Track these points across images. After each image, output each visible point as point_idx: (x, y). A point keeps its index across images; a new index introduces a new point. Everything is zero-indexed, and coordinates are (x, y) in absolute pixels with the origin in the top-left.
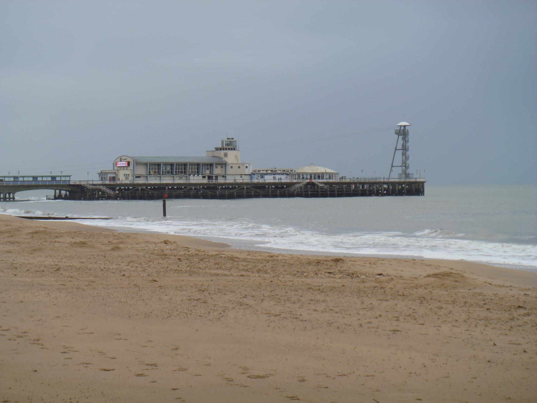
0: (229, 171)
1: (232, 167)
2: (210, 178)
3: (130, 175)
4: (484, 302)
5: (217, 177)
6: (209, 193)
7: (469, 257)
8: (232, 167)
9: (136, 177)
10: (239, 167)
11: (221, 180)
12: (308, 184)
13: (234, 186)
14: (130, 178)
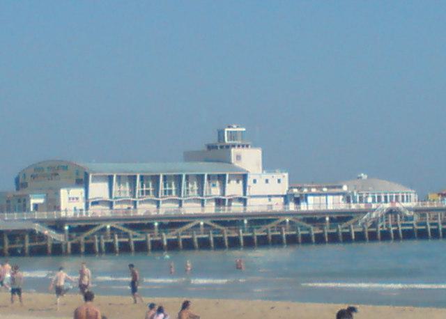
0: (253, 189)
1: (255, 181)
2: (219, 202)
8: (255, 181)
10: (267, 181)
11: (237, 208)
12: (390, 211)
13: (259, 220)
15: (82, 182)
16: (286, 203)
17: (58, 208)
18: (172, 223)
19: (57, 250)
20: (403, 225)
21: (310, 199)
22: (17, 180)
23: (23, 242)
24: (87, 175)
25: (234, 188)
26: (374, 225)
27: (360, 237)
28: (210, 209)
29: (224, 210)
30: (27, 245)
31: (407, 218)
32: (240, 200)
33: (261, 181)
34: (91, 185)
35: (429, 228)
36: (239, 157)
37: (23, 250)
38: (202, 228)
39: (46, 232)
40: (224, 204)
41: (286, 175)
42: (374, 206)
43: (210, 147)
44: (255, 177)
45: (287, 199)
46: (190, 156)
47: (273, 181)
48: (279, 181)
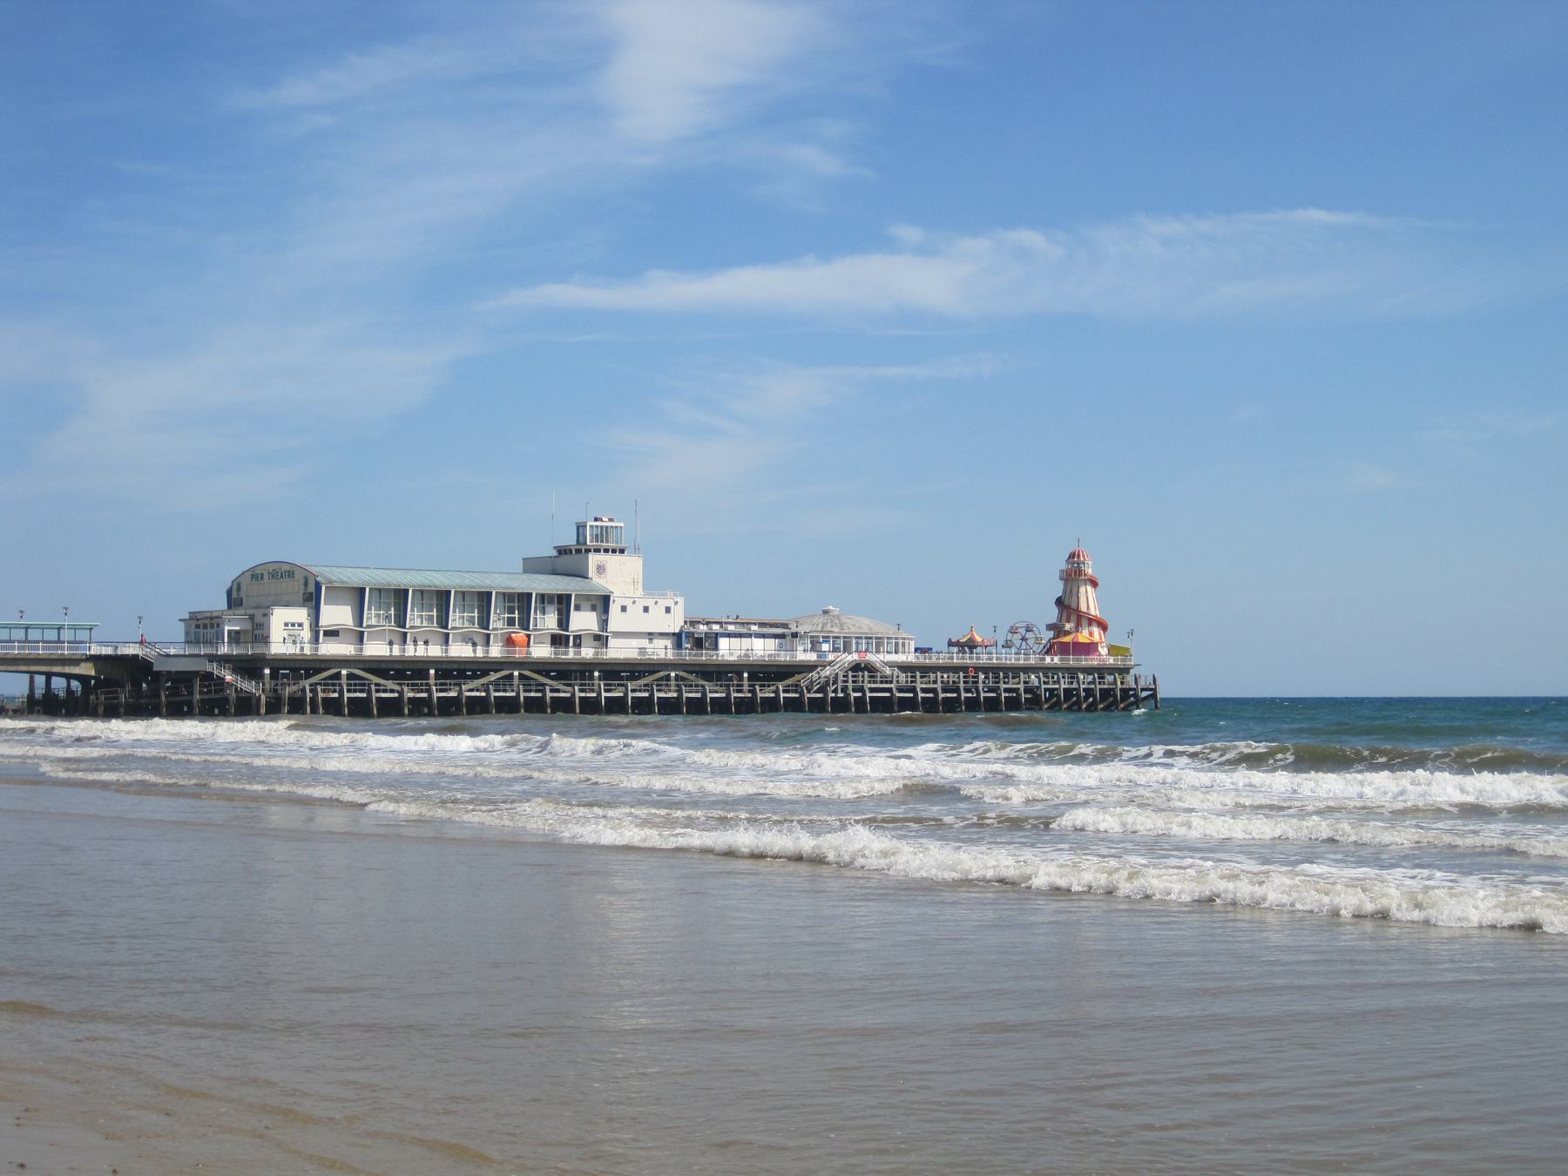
0: (616, 621)
1: (624, 609)
2: (557, 641)
8: (624, 609)
9: (328, 633)
10: (646, 609)
11: (587, 653)
12: (856, 668)
13: (614, 672)
14: (306, 634)
15: (312, 600)
17: (265, 640)
20: (872, 690)
21: (724, 643)
22: (229, 593)
23: (191, 693)
24: (318, 586)
25: (583, 621)
26: (822, 689)
28: (542, 651)
29: (566, 653)
31: (885, 679)
32: (597, 638)
33: (635, 611)
34: (324, 608)
35: (921, 695)
36: (601, 569)
38: (344, 681)
39: (228, 678)
40: (567, 645)
41: (681, 600)
42: (831, 657)
43: (563, 551)
44: (628, 603)
45: (678, 638)
46: (533, 566)
47: (657, 611)
48: (668, 610)
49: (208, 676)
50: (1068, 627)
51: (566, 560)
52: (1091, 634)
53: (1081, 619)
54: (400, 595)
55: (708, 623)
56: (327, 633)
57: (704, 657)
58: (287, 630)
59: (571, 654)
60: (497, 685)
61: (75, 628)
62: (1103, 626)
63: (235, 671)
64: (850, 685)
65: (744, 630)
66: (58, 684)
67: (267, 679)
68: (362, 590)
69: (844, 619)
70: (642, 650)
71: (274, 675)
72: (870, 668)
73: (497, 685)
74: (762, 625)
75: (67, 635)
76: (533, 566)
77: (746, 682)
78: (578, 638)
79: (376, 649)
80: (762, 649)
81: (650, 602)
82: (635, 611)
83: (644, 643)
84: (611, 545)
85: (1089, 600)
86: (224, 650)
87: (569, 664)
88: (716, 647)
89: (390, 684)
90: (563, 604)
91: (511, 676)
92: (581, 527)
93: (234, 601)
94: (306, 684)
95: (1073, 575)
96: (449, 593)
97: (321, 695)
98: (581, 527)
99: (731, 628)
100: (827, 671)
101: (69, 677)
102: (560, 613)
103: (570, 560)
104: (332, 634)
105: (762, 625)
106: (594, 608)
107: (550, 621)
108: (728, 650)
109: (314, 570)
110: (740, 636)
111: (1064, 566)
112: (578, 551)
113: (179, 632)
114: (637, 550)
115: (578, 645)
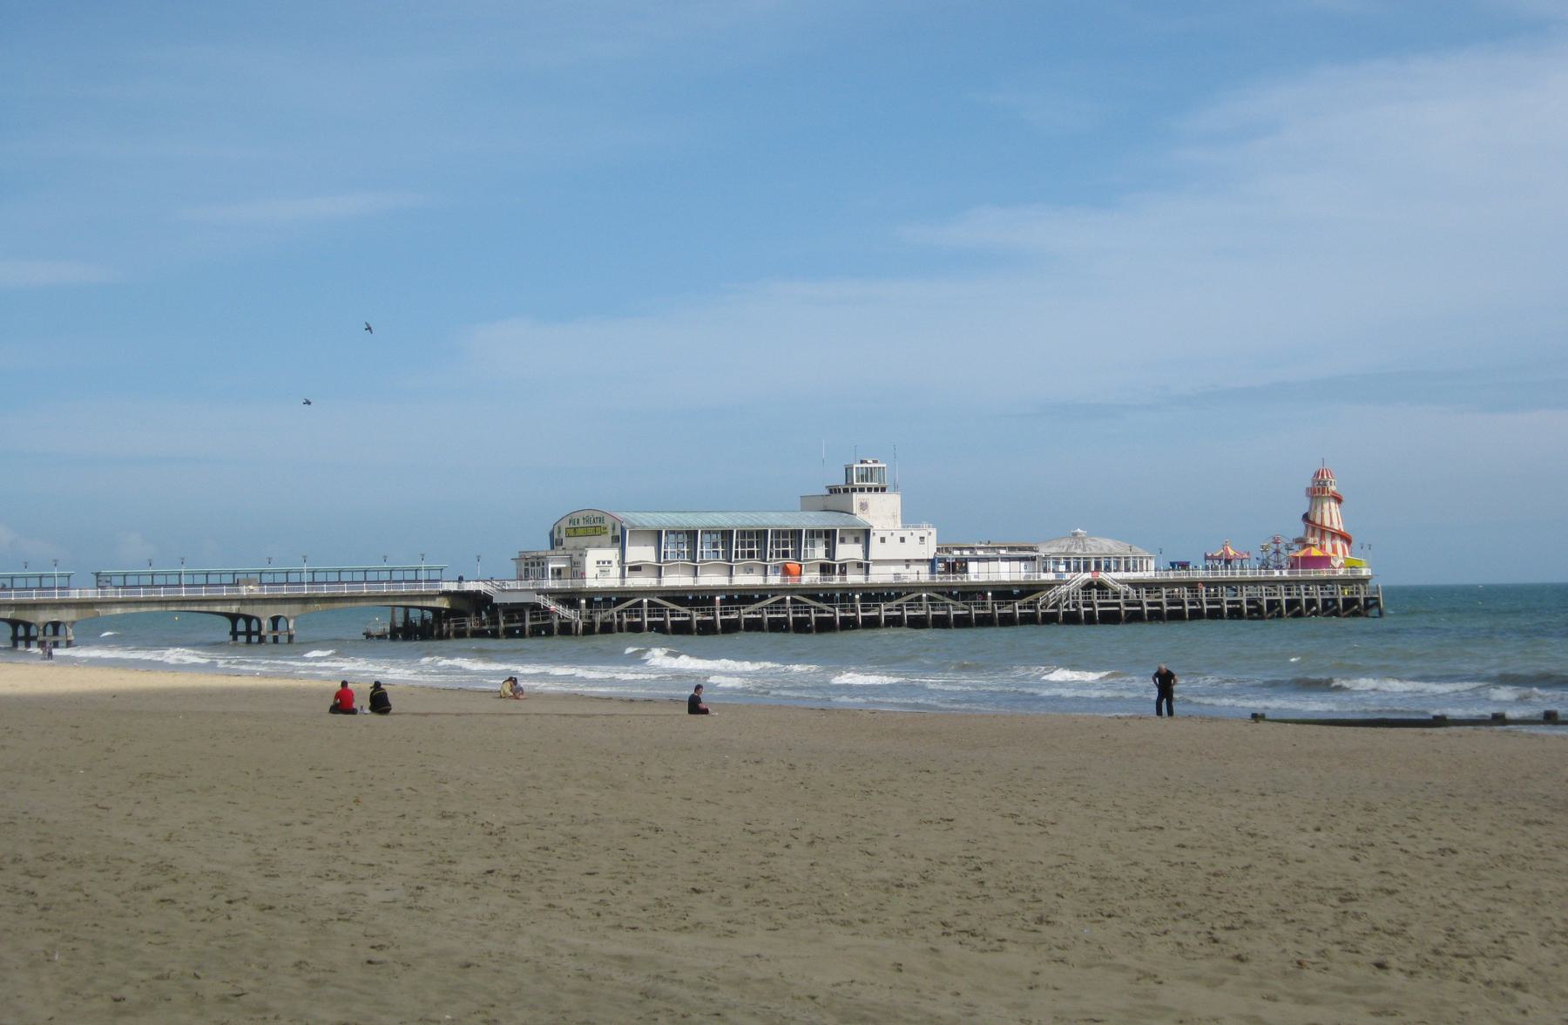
0: (877, 551)
1: (883, 540)
2: (826, 569)
3: (615, 563)
4: (862, 916)
5: (843, 567)
6: (839, 614)
7: (588, 711)
8: (883, 540)
9: (631, 569)
10: (902, 540)
11: (854, 578)
12: (1088, 586)
13: (873, 595)
14: (615, 571)
15: (619, 541)
16: (933, 571)
17: (583, 576)
18: (746, 597)
19: (566, 629)
20: (1101, 605)
21: (973, 567)
22: (552, 534)
26: (1055, 606)
27: (1050, 619)
28: (811, 578)
30: (528, 623)
31: (1116, 595)
32: (860, 565)
33: (893, 541)
35: (1146, 608)
36: (864, 506)
37: (522, 629)
39: (552, 608)
41: (934, 531)
42: (1068, 576)
43: (833, 490)
46: (808, 503)
47: (913, 541)
49: (535, 607)
50: (1311, 540)
51: (838, 499)
52: (1322, 548)
53: (1323, 531)
54: (692, 535)
55: (960, 549)
56: (631, 569)
57: (952, 579)
58: (601, 569)
59: (836, 580)
60: (770, 609)
61: (429, 570)
62: (1347, 539)
63: (559, 602)
64: (1081, 601)
65: (991, 554)
66: (415, 615)
67: (583, 608)
68: (659, 533)
69: (1088, 542)
70: (897, 575)
71: (589, 605)
72: (1101, 586)
73: (910, 606)
74: (1012, 549)
75: (423, 575)
76: (808, 503)
77: (990, 601)
78: (843, 567)
79: (677, 580)
80: (1007, 572)
81: (906, 534)
82: (893, 541)
83: (901, 569)
84: (874, 484)
85: (1332, 515)
86: (551, 584)
87: (835, 589)
88: (965, 570)
89: (684, 610)
90: (829, 536)
91: (783, 601)
92: (848, 470)
93: (555, 543)
94: (614, 611)
95: (1318, 492)
96: (731, 532)
97: (626, 620)
98: (848, 470)
99: (980, 553)
100: (1064, 589)
101: (422, 608)
102: (827, 544)
103: (841, 492)
104: (636, 568)
105: (1012, 549)
106: (857, 541)
107: (819, 552)
108: (977, 573)
109: (620, 515)
110: (988, 560)
111: (1310, 485)
112: (846, 491)
113: (512, 569)
114: (896, 489)
115: (843, 573)
